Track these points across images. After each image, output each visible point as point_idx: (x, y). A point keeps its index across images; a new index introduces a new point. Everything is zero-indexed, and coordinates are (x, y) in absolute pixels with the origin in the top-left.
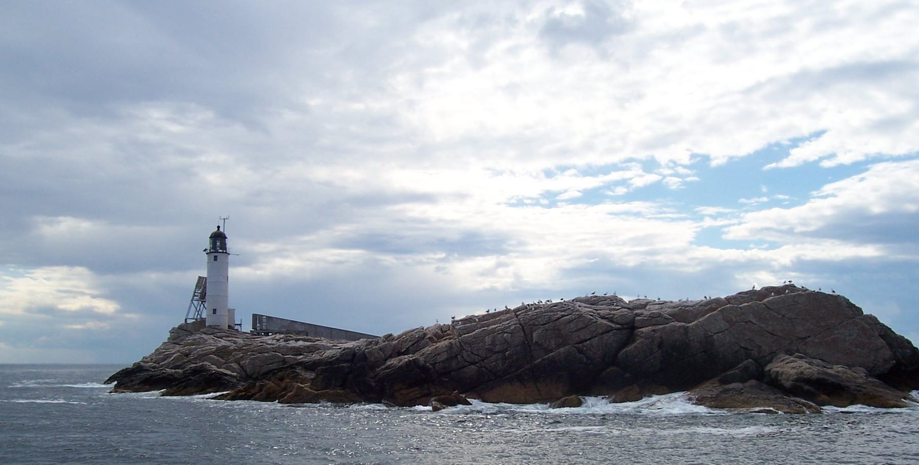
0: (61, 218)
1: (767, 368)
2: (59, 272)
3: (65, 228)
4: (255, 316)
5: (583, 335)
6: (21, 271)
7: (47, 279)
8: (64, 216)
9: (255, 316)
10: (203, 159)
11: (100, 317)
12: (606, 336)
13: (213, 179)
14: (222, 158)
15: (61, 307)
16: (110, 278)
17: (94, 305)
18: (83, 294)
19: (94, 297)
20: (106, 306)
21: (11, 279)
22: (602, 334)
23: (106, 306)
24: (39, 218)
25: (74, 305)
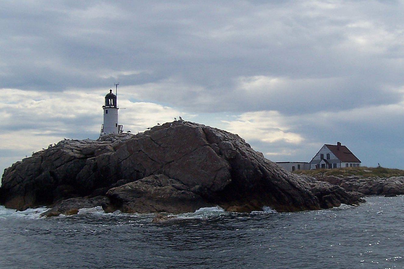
0: (256, 77)
1: (77, 178)
2: (257, 116)
3: (260, 84)
4: (338, 142)
5: (57, 163)
6: (234, 116)
7: (251, 121)
8: (258, 75)
9: (338, 142)
10: (350, 26)
11: (292, 146)
12: (69, 164)
13: (361, 41)
14: (366, 24)
15: (264, 140)
16: (294, 118)
17: (285, 138)
18: (278, 130)
19: (286, 132)
20: (294, 138)
21: (229, 122)
22: (67, 162)
23: (294, 138)
24: (242, 78)
25: (274, 137)
